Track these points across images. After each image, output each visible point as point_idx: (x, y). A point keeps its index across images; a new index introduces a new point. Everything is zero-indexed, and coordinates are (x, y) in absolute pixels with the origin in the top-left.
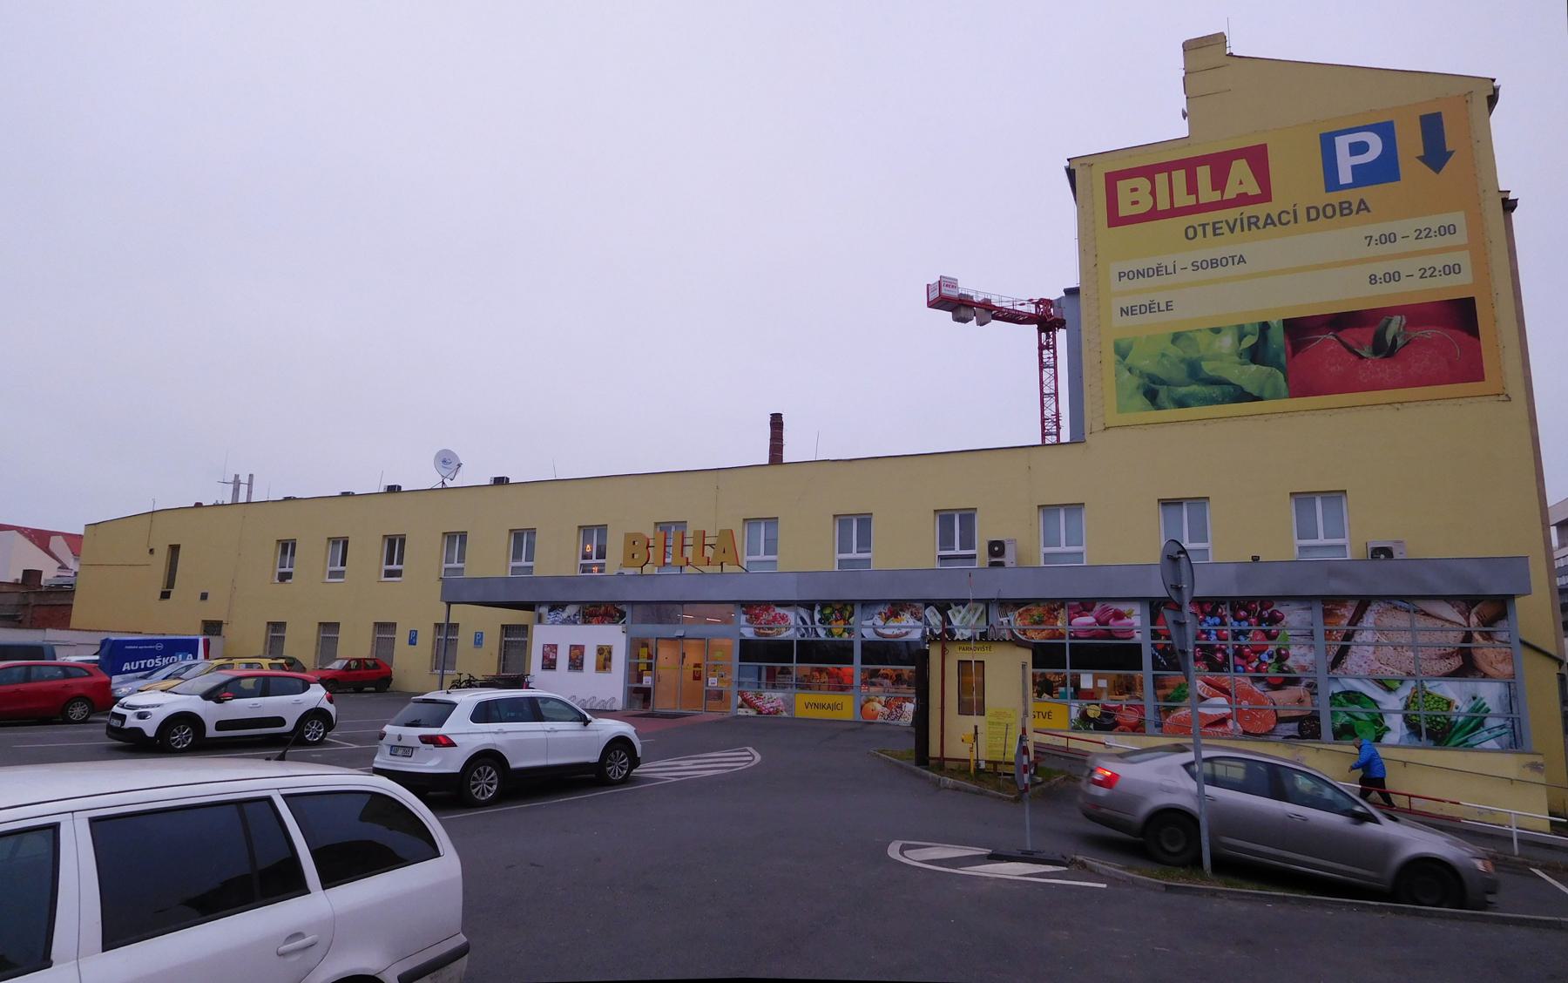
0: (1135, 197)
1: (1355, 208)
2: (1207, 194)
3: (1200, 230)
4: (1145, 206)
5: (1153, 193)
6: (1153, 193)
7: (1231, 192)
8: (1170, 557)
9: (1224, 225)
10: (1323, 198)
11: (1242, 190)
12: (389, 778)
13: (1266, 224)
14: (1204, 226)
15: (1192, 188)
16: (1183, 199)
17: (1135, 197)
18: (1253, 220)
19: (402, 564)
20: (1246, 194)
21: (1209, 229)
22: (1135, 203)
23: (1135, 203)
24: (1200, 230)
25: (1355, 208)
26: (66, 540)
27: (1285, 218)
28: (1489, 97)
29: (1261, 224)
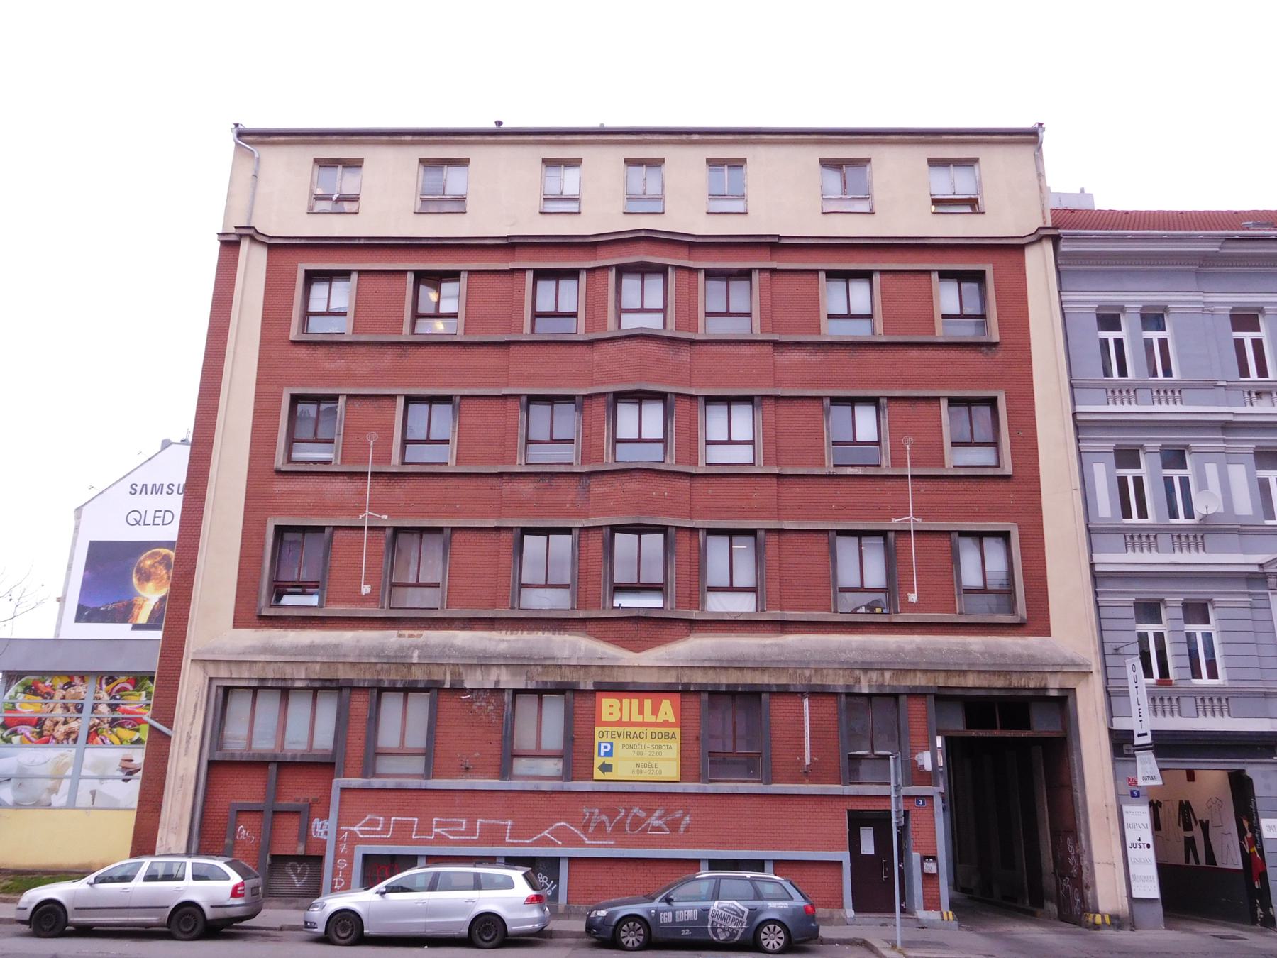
0: (612, 710)
1: (670, 736)
2: (649, 717)
3: (605, 734)
4: (615, 718)
5: (621, 710)
6: (621, 710)
7: (661, 718)
8: (568, 917)
9: (616, 733)
10: (1256, 771)
11: (666, 718)
12: (851, 867)
13: (672, 737)
14: (607, 732)
15: (641, 712)
16: (637, 718)
17: (612, 710)
18: (629, 733)
19: (1186, 838)
20: (668, 721)
21: (609, 734)
22: (611, 714)
23: (611, 714)
24: (605, 734)
25: (670, 736)
26: (150, 730)
27: (642, 735)
28: (59, 599)
29: (632, 736)
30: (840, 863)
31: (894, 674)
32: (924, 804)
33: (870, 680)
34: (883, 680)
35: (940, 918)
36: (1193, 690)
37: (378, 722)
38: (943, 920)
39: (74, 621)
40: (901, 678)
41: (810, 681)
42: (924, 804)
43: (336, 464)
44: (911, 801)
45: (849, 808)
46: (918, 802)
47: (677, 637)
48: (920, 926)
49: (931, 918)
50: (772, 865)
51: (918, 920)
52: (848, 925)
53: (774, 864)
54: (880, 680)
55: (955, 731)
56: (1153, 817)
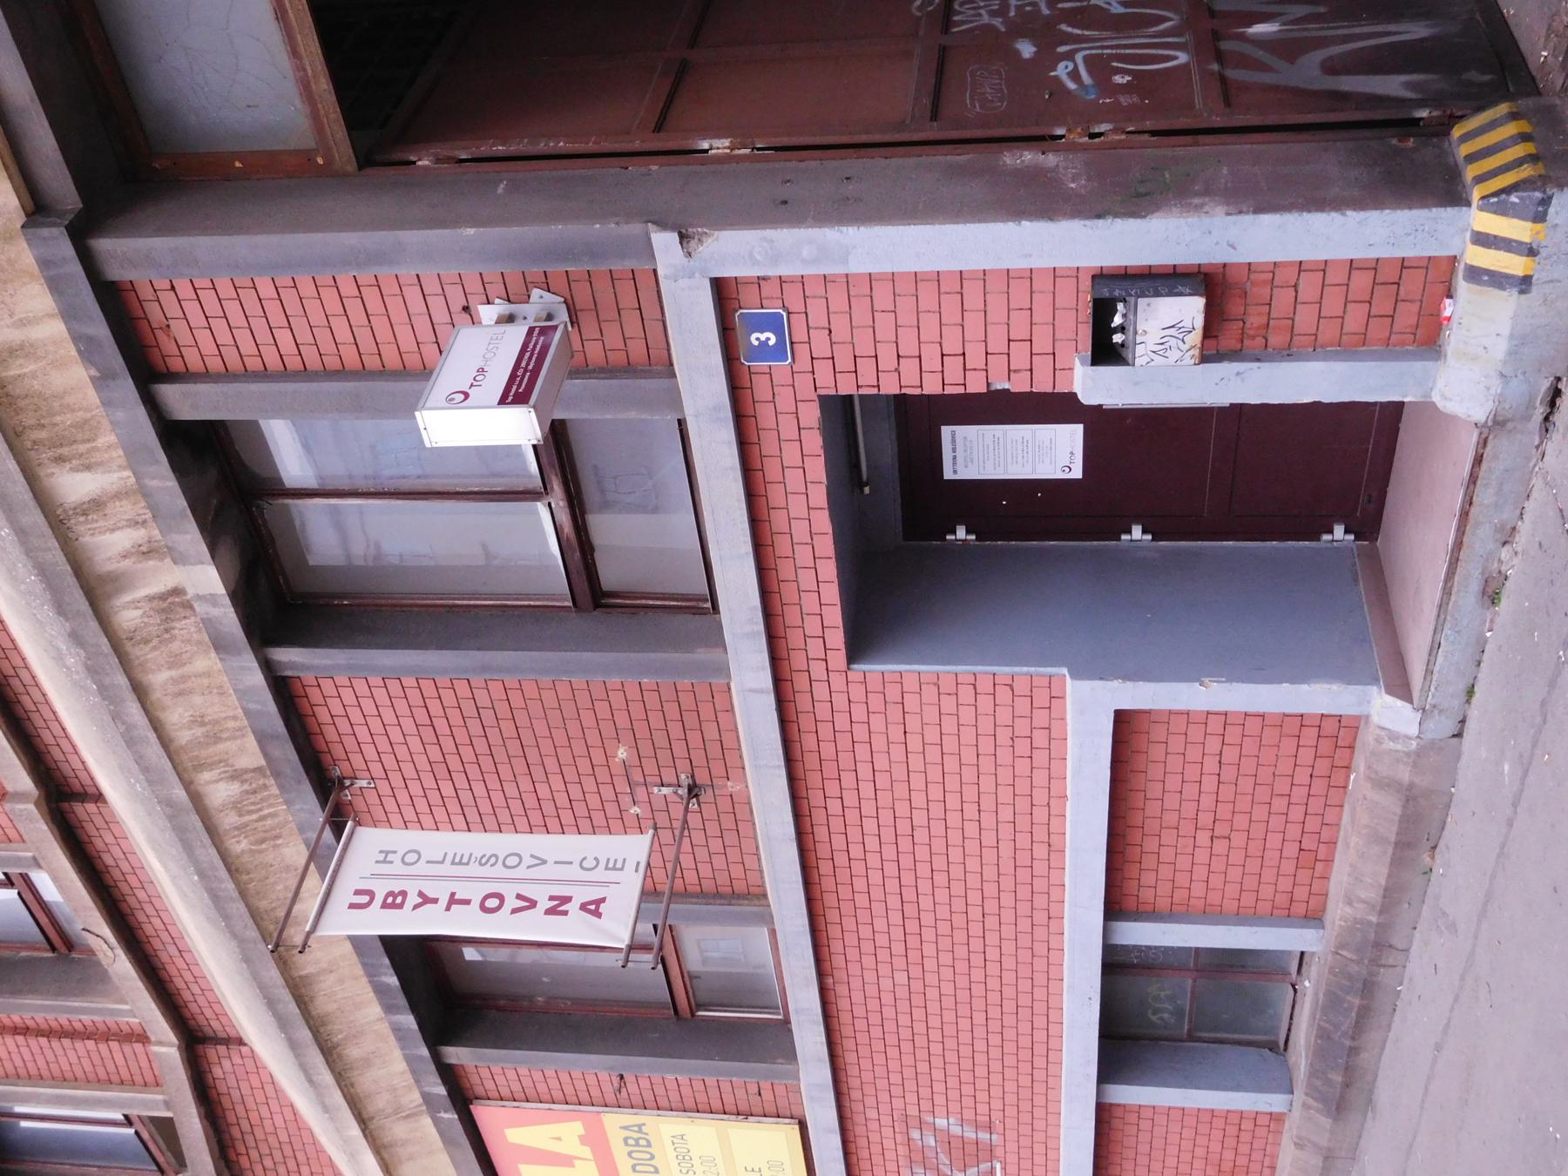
30: (1123, 720)
31: (60, 460)
32: (773, 324)
33: (148, 552)
34: (118, 496)
35: (1505, 304)
36: (1091, 45)
37: (573, 459)
38: (1525, 283)
39: (572, 1169)
40: (68, 419)
41: (258, 770)
42: (773, 324)
43: (168, 1105)
44: (761, 388)
45: (838, 658)
46: (763, 350)
47: (269, 1089)
48: (1540, 412)
49: (1500, 349)
50: (1119, 924)
51: (1497, 424)
52: (1459, 735)
53: (1117, 919)
54: (126, 509)
55: (294, 53)
56: (104, 912)
